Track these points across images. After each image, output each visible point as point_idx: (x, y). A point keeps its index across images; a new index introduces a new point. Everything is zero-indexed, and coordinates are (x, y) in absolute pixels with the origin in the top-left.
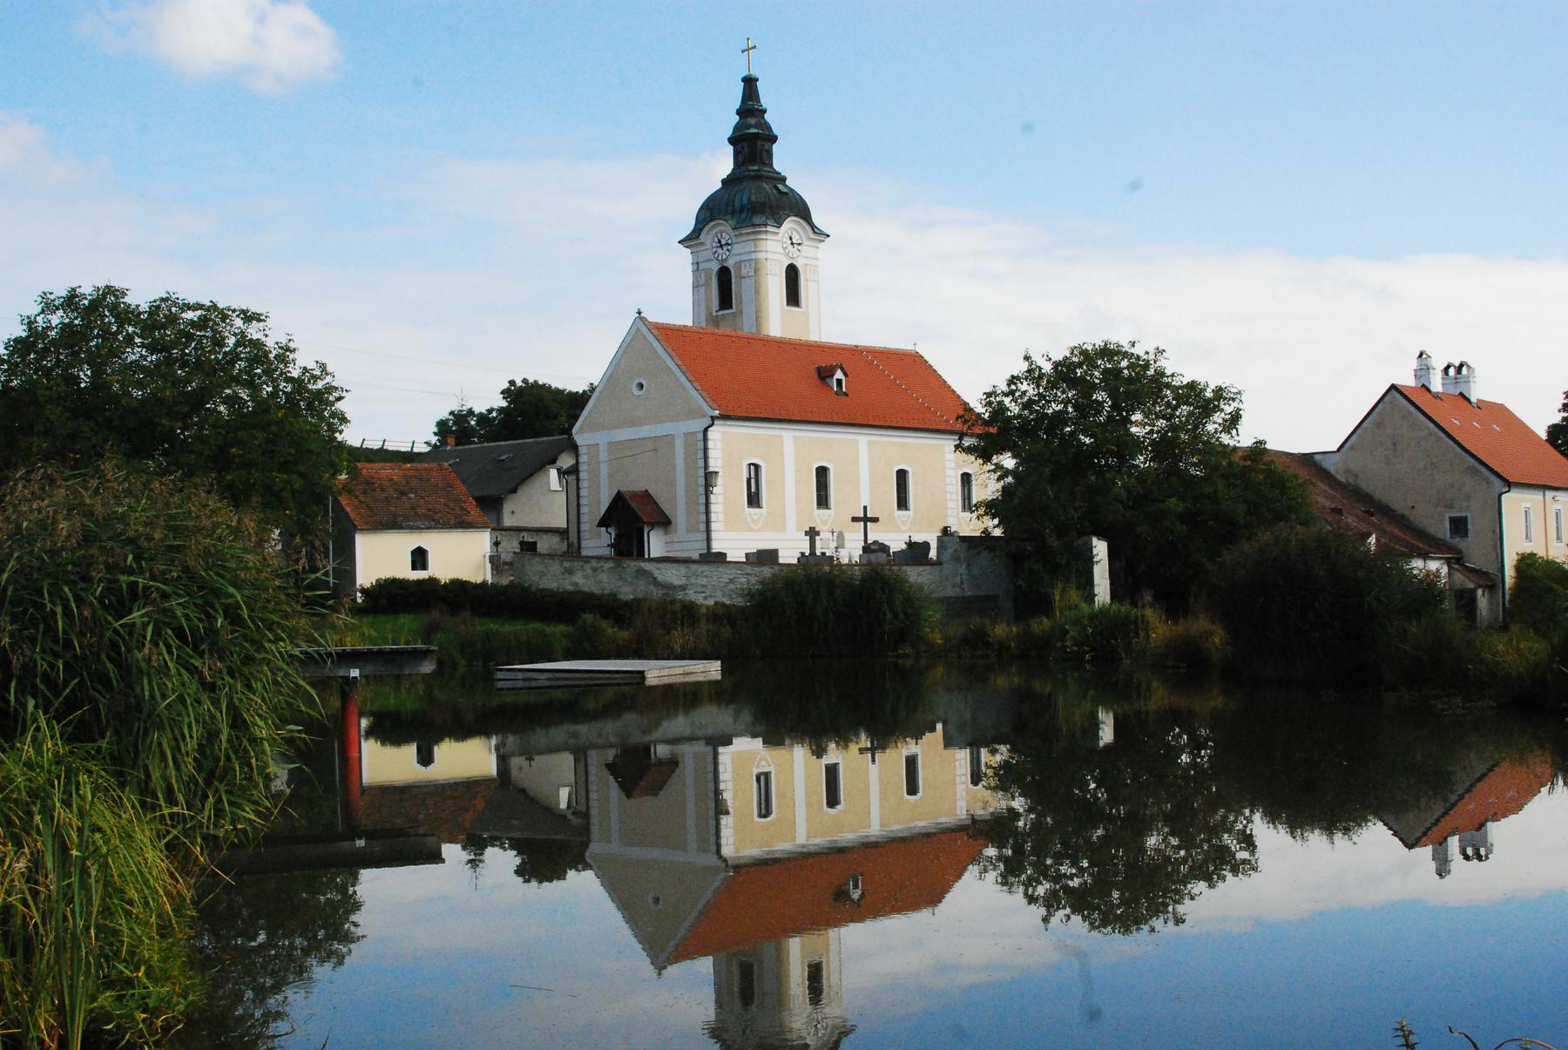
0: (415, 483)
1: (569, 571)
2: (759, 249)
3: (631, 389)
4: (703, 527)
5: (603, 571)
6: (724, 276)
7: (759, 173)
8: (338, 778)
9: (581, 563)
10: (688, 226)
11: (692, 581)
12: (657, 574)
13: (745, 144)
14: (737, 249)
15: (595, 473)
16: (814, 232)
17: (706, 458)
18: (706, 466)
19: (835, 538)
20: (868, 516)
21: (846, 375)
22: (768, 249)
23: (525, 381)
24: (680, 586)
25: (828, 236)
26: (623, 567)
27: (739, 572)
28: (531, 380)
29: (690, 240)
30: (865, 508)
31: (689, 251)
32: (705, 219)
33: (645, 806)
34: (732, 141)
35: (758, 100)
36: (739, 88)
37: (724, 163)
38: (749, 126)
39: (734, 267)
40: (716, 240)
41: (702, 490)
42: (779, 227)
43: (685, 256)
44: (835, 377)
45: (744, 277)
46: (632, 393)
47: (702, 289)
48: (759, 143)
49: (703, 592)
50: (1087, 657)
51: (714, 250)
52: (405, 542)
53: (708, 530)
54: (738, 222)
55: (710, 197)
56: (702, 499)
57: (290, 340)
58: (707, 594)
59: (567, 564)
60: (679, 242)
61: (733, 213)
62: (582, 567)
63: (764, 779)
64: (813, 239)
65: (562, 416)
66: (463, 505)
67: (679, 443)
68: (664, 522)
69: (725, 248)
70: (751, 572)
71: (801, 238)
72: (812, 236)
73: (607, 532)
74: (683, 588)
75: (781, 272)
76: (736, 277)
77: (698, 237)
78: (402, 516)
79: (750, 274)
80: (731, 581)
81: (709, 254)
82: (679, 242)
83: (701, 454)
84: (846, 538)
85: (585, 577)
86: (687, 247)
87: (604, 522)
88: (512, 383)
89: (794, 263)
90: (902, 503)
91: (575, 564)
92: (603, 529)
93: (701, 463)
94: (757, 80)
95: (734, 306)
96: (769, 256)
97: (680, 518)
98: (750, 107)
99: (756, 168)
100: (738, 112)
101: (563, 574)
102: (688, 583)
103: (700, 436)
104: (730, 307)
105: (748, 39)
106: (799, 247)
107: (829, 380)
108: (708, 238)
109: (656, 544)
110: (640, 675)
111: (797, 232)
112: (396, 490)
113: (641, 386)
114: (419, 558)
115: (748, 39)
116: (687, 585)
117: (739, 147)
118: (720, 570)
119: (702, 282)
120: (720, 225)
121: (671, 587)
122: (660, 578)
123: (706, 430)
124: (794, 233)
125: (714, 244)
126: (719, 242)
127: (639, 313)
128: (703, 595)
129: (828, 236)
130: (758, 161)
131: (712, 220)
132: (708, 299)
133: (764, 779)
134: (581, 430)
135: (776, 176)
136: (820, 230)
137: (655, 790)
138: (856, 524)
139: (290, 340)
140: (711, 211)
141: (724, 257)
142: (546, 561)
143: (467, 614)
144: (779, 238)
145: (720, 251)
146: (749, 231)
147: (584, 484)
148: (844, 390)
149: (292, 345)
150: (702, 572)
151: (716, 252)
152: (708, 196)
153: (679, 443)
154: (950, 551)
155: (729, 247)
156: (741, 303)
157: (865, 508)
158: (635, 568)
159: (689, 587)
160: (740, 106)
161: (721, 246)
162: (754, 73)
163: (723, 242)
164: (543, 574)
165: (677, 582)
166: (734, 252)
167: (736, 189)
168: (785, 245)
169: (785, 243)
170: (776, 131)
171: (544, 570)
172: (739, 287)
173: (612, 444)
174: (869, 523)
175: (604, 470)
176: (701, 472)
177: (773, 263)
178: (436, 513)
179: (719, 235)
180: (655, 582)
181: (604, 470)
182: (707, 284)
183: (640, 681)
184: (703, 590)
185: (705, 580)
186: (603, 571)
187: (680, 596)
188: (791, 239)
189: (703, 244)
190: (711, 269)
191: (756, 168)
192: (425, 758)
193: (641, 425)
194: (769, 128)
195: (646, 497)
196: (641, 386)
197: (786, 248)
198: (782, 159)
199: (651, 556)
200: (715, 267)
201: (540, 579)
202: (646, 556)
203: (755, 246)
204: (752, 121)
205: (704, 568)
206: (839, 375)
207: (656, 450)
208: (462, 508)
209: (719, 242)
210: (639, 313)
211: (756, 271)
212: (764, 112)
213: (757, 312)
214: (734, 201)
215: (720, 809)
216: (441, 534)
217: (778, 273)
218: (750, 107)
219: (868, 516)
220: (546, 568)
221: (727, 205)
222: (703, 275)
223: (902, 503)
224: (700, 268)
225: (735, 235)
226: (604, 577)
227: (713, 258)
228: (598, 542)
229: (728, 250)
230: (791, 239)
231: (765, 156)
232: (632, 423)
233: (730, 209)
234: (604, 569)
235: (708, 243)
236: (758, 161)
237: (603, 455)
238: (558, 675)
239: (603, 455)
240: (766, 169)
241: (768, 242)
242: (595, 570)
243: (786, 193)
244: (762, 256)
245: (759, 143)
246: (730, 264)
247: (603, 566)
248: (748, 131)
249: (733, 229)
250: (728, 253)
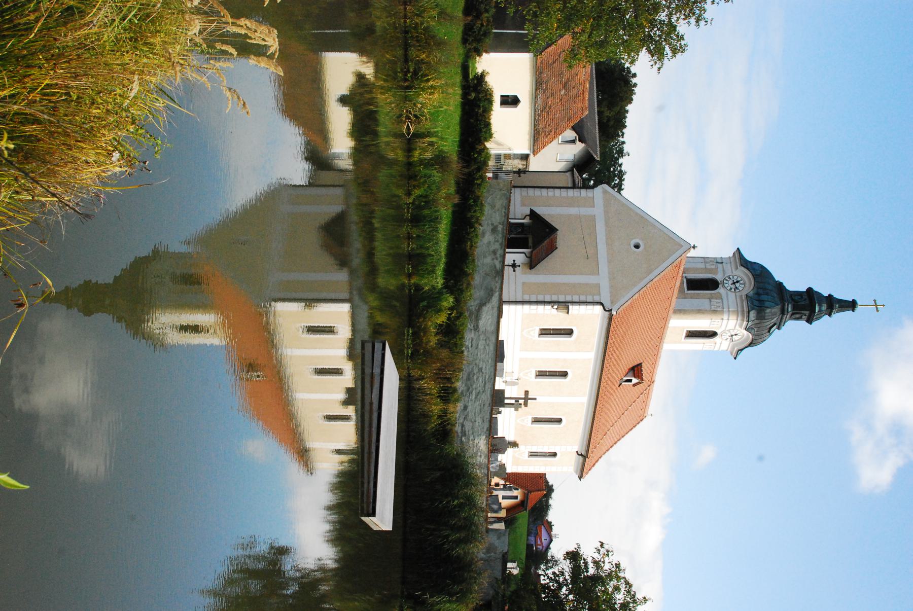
0: (573, 93)
1: (494, 230)
2: (730, 313)
3: (635, 238)
4: (526, 298)
5: (493, 259)
6: (710, 284)
7: (786, 312)
8: (326, 31)
9: (500, 241)
10: (750, 257)
11: (482, 337)
12: (489, 306)
13: (807, 302)
14: (732, 296)
15: (571, 203)
16: (739, 351)
17: (580, 303)
18: (573, 303)
19: (514, 380)
20: (529, 401)
21: (634, 385)
22: (730, 321)
23: (635, 85)
24: (478, 326)
25: (735, 358)
26: (495, 277)
27: (487, 377)
28: (636, 90)
29: (740, 259)
30: (535, 399)
31: (731, 255)
32: (754, 269)
33: (312, 239)
34: (810, 290)
35: (839, 311)
36: (849, 298)
37: (794, 284)
38: (820, 306)
39: (719, 293)
40: (739, 279)
41: (554, 298)
42: (745, 329)
43: (727, 252)
44: (633, 379)
45: (710, 301)
46: (632, 239)
47: (703, 266)
48: (807, 313)
49: (472, 346)
50: (472, 89)
51: (731, 277)
52: (523, 88)
53: (523, 302)
54: (751, 297)
55: (770, 273)
56: (548, 299)
57: (706, 21)
58: (470, 349)
59: (500, 228)
60: (738, 249)
61: (758, 294)
62: (497, 241)
63: (329, 330)
64: (734, 348)
65: (610, 113)
66: (553, 132)
67: (591, 280)
68: (532, 264)
69: (733, 286)
70: (487, 387)
71: (736, 341)
72: (736, 349)
73: (526, 216)
74: (476, 328)
75: (712, 328)
76: (711, 294)
77: (742, 265)
78: (547, 88)
79: (712, 307)
80: (480, 370)
81: (728, 273)
82: (738, 249)
83: (583, 298)
84: (513, 387)
85: (489, 243)
86: (734, 254)
87: (533, 215)
88: (634, 75)
89: (717, 336)
90: (536, 421)
91: (500, 235)
92: (529, 213)
93: (576, 299)
94: (853, 311)
95: (690, 292)
96: (725, 321)
97: (536, 277)
98: (833, 305)
99: (790, 309)
100: (830, 296)
101: (492, 224)
102: (480, 333)
103: (597, 299)
104: (689, 289)
105: (883, 305)
106: (729, 340)
107: (631, 373)
108: (742, 274)
109: (516, 256)
110: (371, 511)
111: (740, 339)
112: (568, 79)
113: (637, 247)
114: (510, 101)
115: (883, 305)
116: (478, 331)
117: (805, 297)
118: (490, 361)
119: (708, 266)
120: (751, 284)
121: (478, 318)
122: (485, 309)
123: (602, 304)
124: (740, 337)
125: (735, 277)
126: (738, 282)
127: (694, 247)
128: (470, 345)
129: (735, 358)
130: (794, 312)
131: (753, 276)
132: (696, 270)
133: (329, 330)
134: (605, 192)
135: (782, 324)
136: (739, 354)
137: (326, 247)
138: (523, 393)
139: (706, 21)
140: (760, 273)
141: (726, 285)
142: (504, 210)
143: (456, 200)
144: (737, 327)
145: (731, 282)
146: (745, 308)
147: (564, 192)
148: (623, 383)
149: (702, 23)
150: (488, 345)
151: (730, 278)
152: (768, 269)
153: (591, 280)
154: (497, 543)
155: (733, 290)
156: (691, 298)
157: (535, 399)
158: (494, 288)
159: (477, 333)
160: (835, 298)
161: (734, 283)
162: (858, 309)
163: (737, 285)
164: (493, 206)
165: (481, 323)
166: (729, 292)
167: (775, 295)
168: (731, 331)
169: (733, 331)
170: (814, 323)
171: (496, 208)
172: (704, 297)
173: (593, 219)
174: (523, 400)
175: (573, 211)
176: (569, 298)
177: (720, 324)
178: (548, 113)
179: (742, 282)
180: (482, 305)
181: (573, 211)
182: (706, 270)
183: (365, 512)
184: (474, 345)
185: (482, 347)
186: (493, 259)
187: (470, 326)
188: (736, 335)
189: (737, 268)
190: (716, 273)
191: (790, 309)
192: (343, 100)
193: (608, 244)
194: (817, 319)
195: (552, 248)
196: (637, 247)
197: (730, 332)
198: (794, 328)
199: (507, 254)
200: (719, 277)
201: (489, 204)
202: (508, 250)
203: (733, 312)
204: (824, 307)
205: (492, 347)
206: (635, 381)
207: (588, 258)
208: (551, 131)
209: (738, 282)
210: (694, 247)
211: (715, 312)
212: (830, 315)
213: (684, 310)
214: (767, 294)
215: (310, 302)
216: (529, 84)
217: (712, 326)
218: (833, 305)
219: (529, 401)
220: (498, 210)
221: (765, 289)
222: (713, 267)
223: (536, 421)
224: (718, 264)
225: (742, 296)
226: (488, 260)
227: (726, 276)
228: (519, 212)
229: (731, 289)
230: (736, 335)
231: (798, 316)
232: (608, 237)
233: (761, 291)
234: (495, 260)
235: (735, 273)
236: (794, 312)
237: (584, 211)
238: (375, 415)
239: (584, 211)
240: (788, 316)
241: (736, 321)
242: (494, 252)
243: (769, 332)
244: (725, 317)
245: (807, 313)
246: (721, 290)
247: (497, 259)
248: (817, 305)
249: (746, 295)
250: (729, 288)
